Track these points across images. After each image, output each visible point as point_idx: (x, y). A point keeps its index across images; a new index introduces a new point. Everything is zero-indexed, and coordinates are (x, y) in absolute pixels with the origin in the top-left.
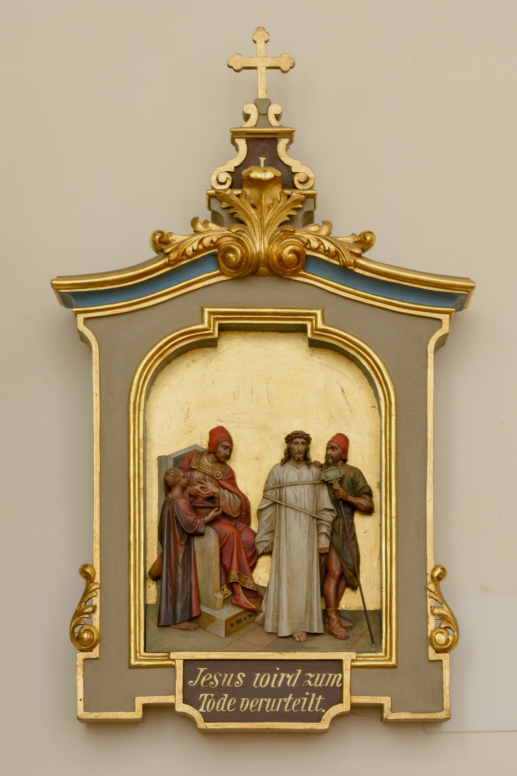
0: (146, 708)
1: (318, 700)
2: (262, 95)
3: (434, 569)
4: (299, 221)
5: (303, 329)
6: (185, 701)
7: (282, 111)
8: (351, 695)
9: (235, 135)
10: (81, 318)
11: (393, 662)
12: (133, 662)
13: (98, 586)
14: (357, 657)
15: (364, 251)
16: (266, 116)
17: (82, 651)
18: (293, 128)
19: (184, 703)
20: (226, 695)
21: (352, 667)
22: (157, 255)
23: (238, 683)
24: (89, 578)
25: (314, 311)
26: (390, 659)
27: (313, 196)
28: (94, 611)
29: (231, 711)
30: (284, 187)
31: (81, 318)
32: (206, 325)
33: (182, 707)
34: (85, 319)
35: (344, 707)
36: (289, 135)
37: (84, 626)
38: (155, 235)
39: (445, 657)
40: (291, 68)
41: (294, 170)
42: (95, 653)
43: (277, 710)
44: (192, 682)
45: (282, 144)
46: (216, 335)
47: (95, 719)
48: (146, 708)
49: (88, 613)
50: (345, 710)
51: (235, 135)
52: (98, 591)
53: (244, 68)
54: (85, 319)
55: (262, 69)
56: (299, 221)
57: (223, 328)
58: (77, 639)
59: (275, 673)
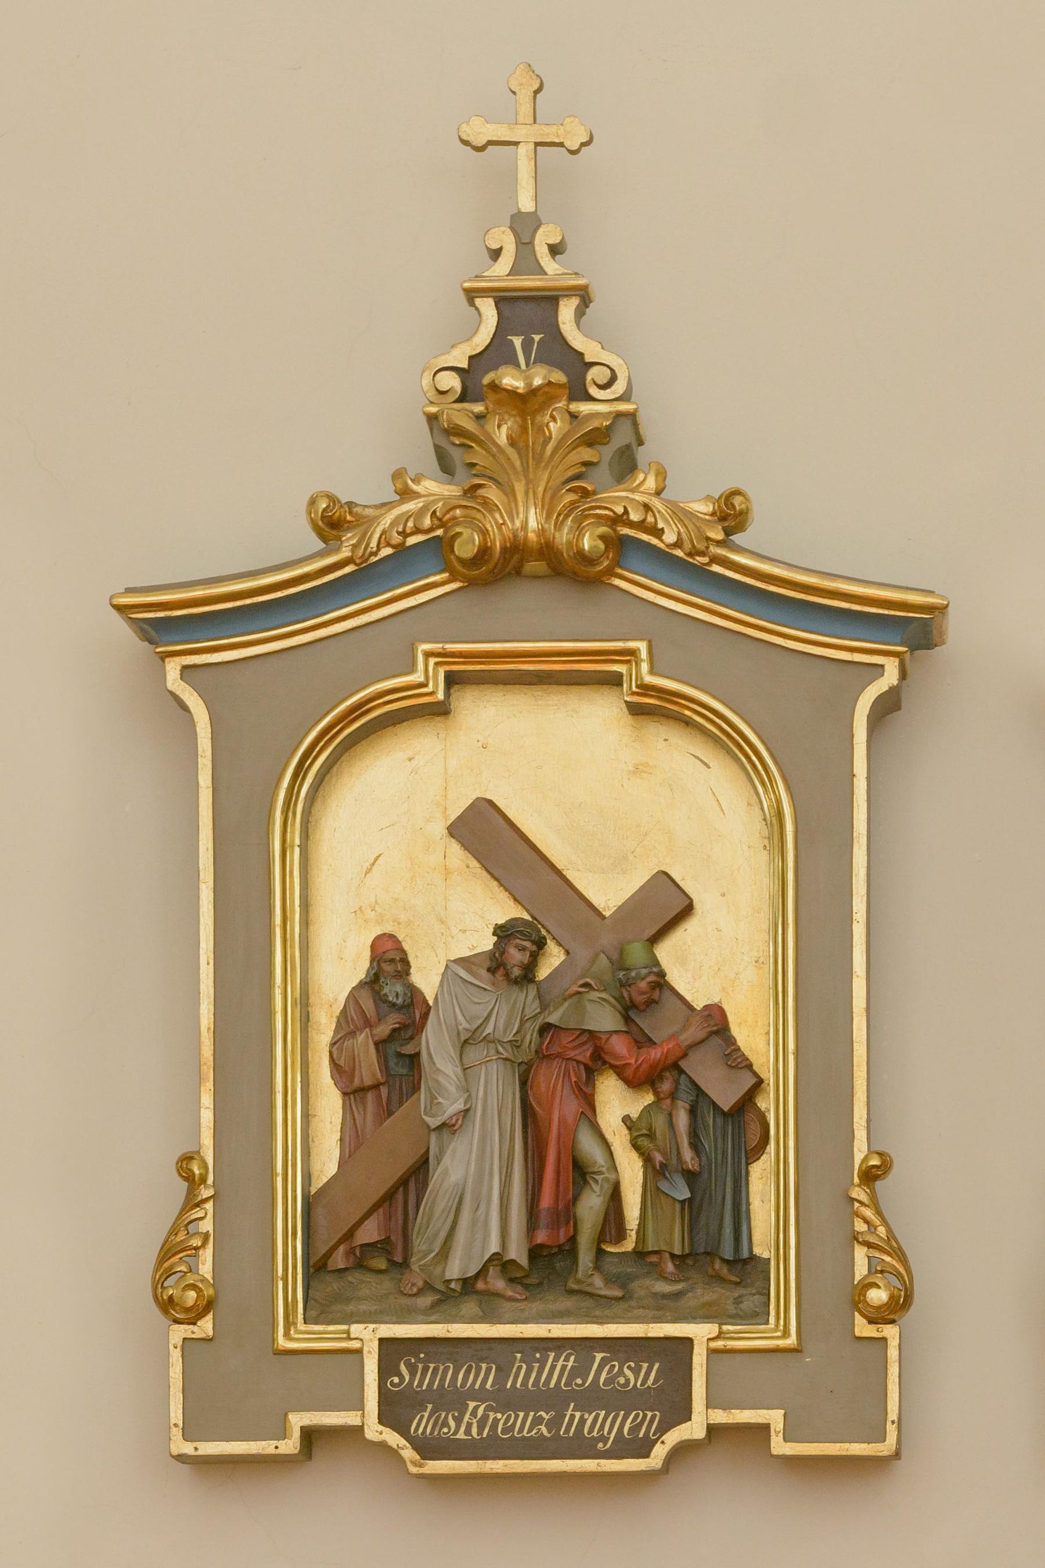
0: (309, 1435)
1: (572, 1411)
2: (526, 204)
3: (865, 1159)
4: (603, 473)
5: (615, 681)
6: (383, 1419)
7: (563, 236)
8: (708, 1406)
9: (471, 295)
10: (173, 668)
11: (792, 1341)
12: (282, 1343)
13: (210, 1192)
14: (720, 1333)
15: (728, 532)
16: (530, 245)
17: (177, 1321)
18: (942, 597)
19: (690, 1419)
20: (430, 1406)
21: (712, 1352)
22: (325, 546)
23: (396, 1380)
24: (193, 1182)
25: (632, 644)
26: (786, 1334)
27: (632, 416)
28: (204, 1245)
29: (503, 1437)
30: (572, 398)
31: (173, 668)
32: (418, 677)
33: (374, 1431)
34: (185, 668)
35: (694, 1429)
36: (584, 296)
37: (188, 1274)
38: (313, 502)
39: (891, 1332)
40: (583, 145)
41: (588, 359)
42: (206, 1326)
43: (571, 1434)
44: (579, 1381)
45: (566, 311)
46: (440, 696)
47: (195, 1456)
48: (309, 1435)
49: (196, 1249)
50: (696, 1437)
51: (471, 295)
52: (209, 1206)
53: (491, 143)
54: (185, 668)
55: (524, 152)
56: (603, 473)
57: (452, 680)
58: (167, 1305)
59: (657, 1362)
